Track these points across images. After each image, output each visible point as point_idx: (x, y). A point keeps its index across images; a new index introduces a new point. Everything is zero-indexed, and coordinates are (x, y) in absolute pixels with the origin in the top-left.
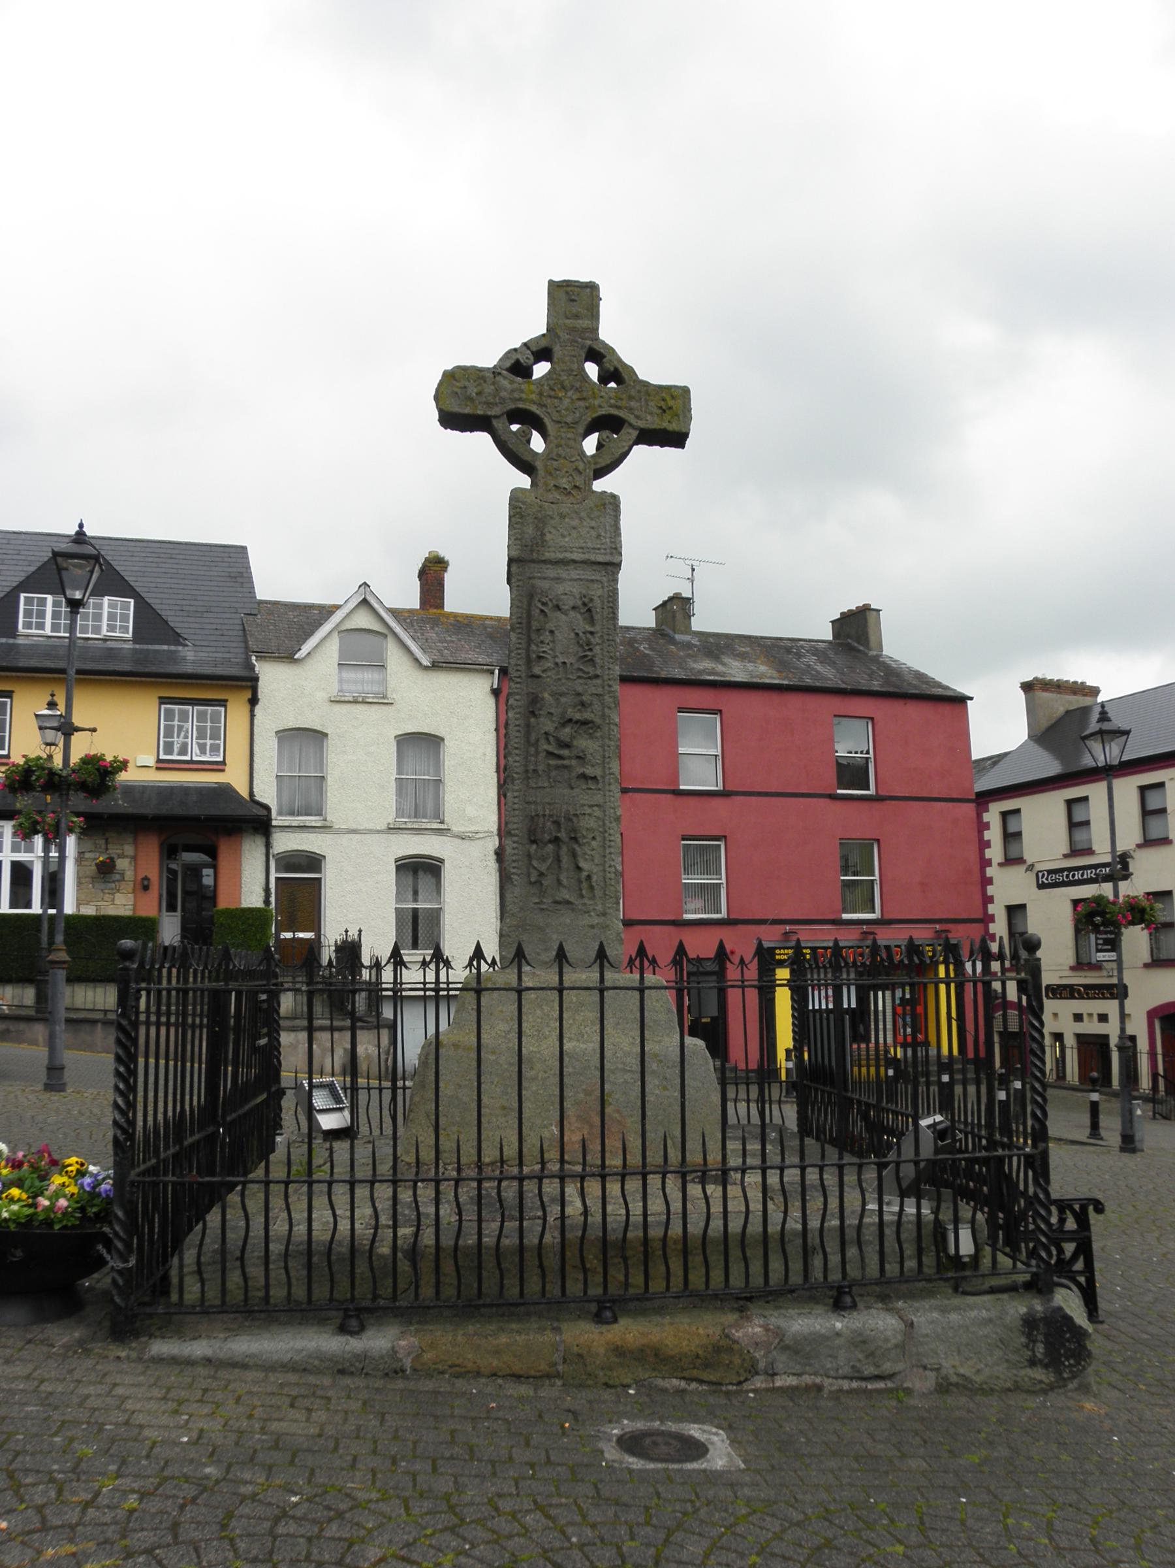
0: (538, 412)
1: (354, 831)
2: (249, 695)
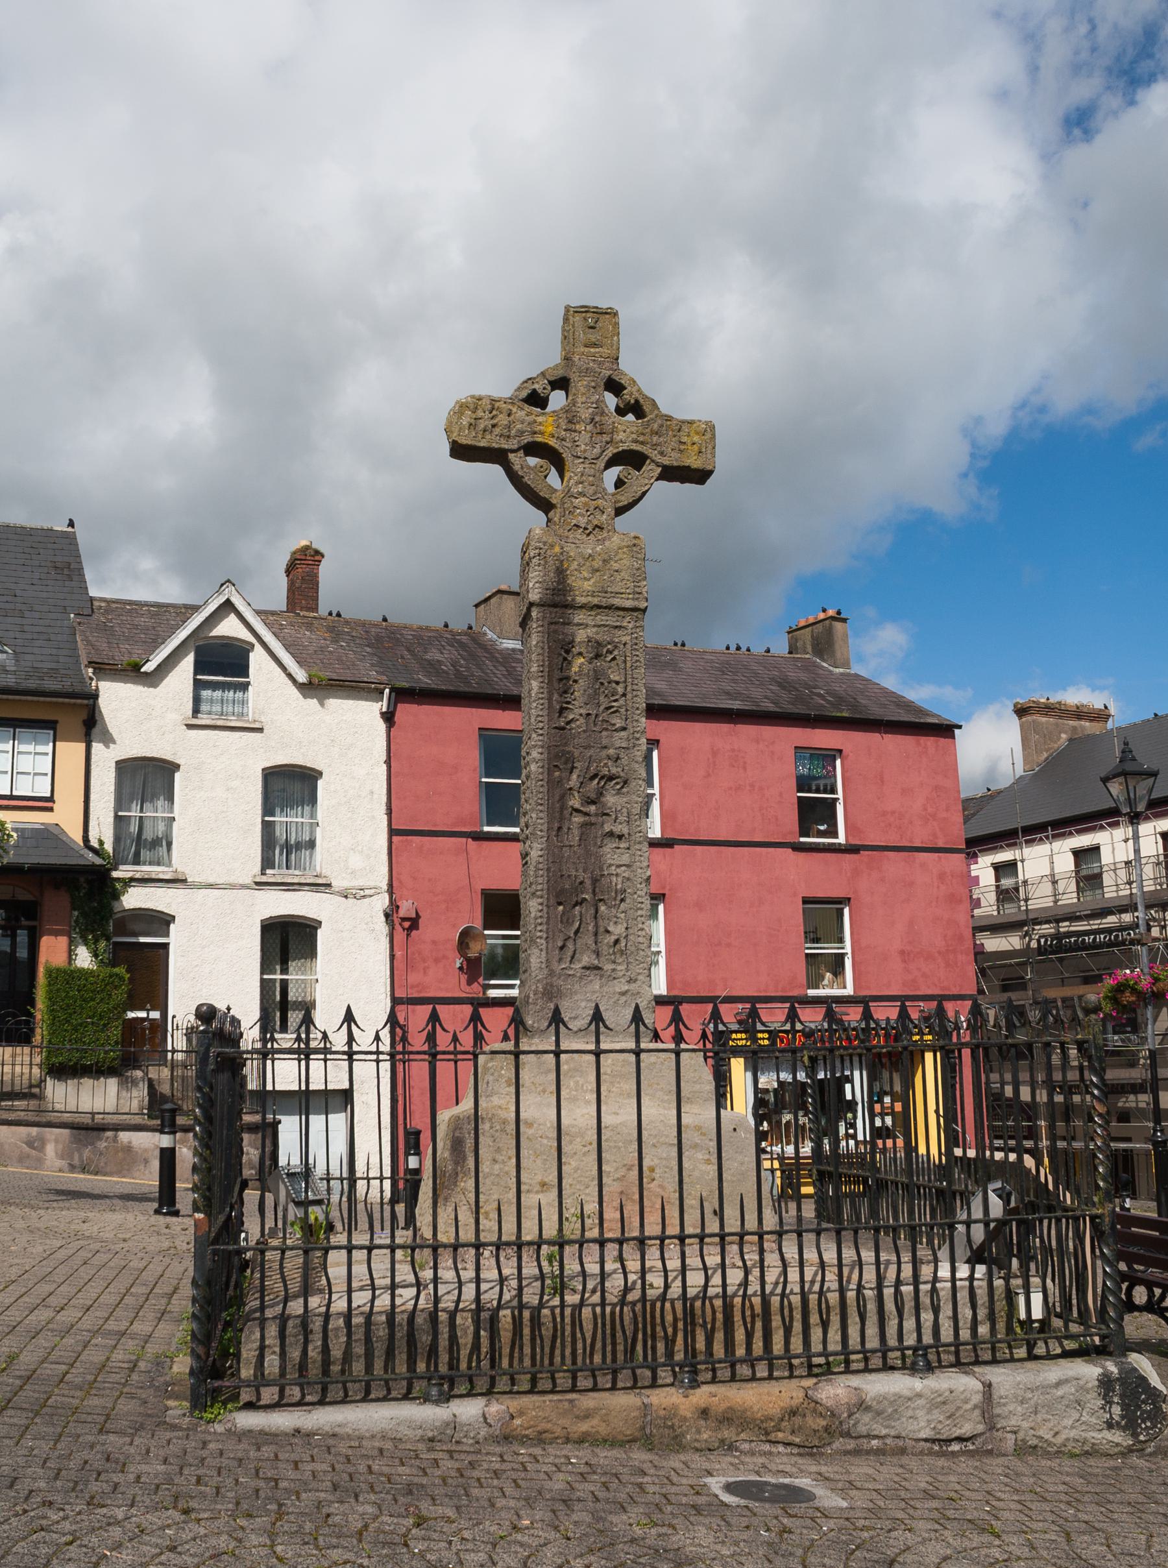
0: (556, 446)
1: (211, 886)
2: (84, 715)
